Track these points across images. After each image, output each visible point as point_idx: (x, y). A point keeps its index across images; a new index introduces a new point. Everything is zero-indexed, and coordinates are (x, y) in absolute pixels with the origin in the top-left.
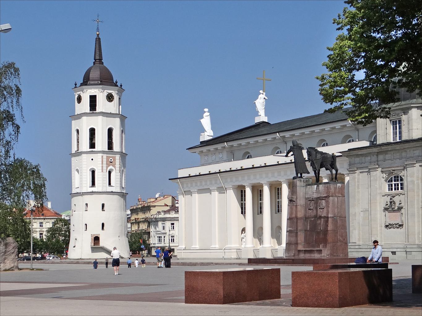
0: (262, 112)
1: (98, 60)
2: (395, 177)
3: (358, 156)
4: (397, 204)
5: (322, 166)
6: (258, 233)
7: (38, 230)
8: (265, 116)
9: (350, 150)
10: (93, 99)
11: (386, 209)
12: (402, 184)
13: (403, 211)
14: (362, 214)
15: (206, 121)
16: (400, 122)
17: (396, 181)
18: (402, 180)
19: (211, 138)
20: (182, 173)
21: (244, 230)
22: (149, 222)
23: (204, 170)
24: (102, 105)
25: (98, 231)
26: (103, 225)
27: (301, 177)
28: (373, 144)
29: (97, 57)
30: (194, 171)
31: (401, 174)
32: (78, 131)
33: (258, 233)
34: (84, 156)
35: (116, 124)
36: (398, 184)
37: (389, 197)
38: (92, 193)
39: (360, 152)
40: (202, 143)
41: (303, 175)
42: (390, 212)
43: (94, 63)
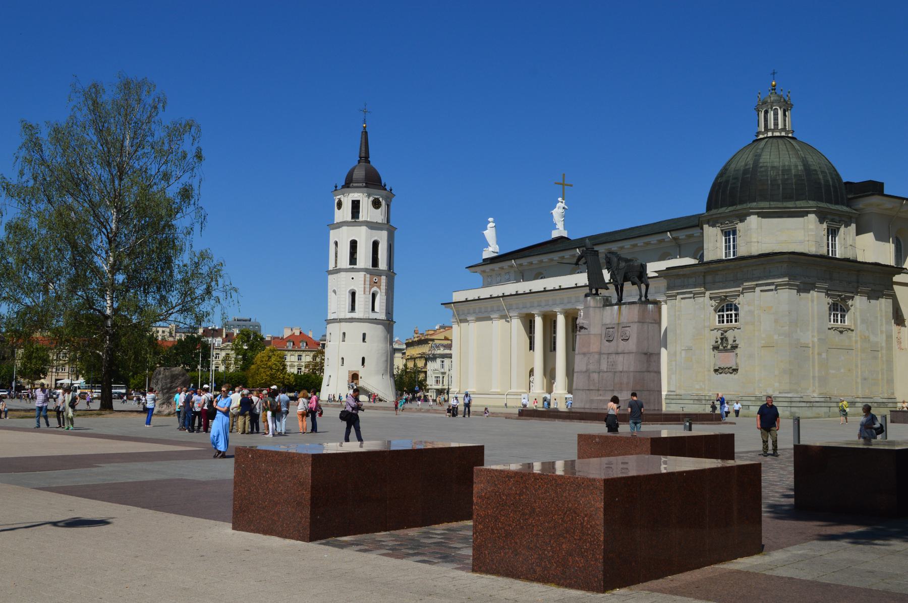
0: (560, 225)
1: (365, 158)
2: (727, 305)
3: (678, 276)
4: (730, 342)
5: (626, 279)
6: (549, 373)
7: (296, 364)
8: (565, 229)
9: (668, 269)
10: (356, 205)
11: (715, 348)
12: (736, 315)
13: (738, 351)
14: (683, 352)
15: (490, 233)
16: (734, 233)
17: (727, 308)
18: (736, 309)
19: (496, 255)
20: (458, 296)
21: (531, 372)
22: (428, 358)
23: (485, 293)
24: (367, 212)
25: (357, 367)
26: (363, 359)
27: (597, 294)
28: (702, 263)
29: (363, 155)
30: (472, 294)
31: (736, 302)
32: (336, 243)
33: (549, 373)
34: (343, 274)
35: (382, 237)
36: (731, 315)
37: (720, 332)
38: (351, 320)
39: (681, 272)
40: (484, 260)
41: (600, 291)
42: (720, 351)
43: (359, 162)
